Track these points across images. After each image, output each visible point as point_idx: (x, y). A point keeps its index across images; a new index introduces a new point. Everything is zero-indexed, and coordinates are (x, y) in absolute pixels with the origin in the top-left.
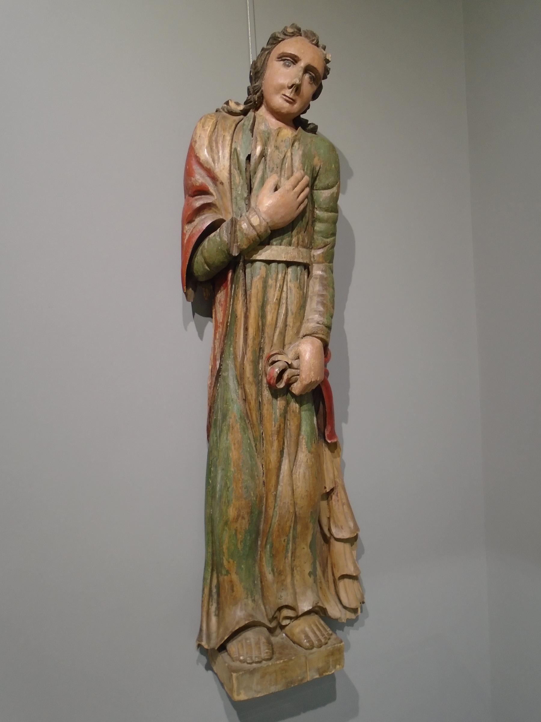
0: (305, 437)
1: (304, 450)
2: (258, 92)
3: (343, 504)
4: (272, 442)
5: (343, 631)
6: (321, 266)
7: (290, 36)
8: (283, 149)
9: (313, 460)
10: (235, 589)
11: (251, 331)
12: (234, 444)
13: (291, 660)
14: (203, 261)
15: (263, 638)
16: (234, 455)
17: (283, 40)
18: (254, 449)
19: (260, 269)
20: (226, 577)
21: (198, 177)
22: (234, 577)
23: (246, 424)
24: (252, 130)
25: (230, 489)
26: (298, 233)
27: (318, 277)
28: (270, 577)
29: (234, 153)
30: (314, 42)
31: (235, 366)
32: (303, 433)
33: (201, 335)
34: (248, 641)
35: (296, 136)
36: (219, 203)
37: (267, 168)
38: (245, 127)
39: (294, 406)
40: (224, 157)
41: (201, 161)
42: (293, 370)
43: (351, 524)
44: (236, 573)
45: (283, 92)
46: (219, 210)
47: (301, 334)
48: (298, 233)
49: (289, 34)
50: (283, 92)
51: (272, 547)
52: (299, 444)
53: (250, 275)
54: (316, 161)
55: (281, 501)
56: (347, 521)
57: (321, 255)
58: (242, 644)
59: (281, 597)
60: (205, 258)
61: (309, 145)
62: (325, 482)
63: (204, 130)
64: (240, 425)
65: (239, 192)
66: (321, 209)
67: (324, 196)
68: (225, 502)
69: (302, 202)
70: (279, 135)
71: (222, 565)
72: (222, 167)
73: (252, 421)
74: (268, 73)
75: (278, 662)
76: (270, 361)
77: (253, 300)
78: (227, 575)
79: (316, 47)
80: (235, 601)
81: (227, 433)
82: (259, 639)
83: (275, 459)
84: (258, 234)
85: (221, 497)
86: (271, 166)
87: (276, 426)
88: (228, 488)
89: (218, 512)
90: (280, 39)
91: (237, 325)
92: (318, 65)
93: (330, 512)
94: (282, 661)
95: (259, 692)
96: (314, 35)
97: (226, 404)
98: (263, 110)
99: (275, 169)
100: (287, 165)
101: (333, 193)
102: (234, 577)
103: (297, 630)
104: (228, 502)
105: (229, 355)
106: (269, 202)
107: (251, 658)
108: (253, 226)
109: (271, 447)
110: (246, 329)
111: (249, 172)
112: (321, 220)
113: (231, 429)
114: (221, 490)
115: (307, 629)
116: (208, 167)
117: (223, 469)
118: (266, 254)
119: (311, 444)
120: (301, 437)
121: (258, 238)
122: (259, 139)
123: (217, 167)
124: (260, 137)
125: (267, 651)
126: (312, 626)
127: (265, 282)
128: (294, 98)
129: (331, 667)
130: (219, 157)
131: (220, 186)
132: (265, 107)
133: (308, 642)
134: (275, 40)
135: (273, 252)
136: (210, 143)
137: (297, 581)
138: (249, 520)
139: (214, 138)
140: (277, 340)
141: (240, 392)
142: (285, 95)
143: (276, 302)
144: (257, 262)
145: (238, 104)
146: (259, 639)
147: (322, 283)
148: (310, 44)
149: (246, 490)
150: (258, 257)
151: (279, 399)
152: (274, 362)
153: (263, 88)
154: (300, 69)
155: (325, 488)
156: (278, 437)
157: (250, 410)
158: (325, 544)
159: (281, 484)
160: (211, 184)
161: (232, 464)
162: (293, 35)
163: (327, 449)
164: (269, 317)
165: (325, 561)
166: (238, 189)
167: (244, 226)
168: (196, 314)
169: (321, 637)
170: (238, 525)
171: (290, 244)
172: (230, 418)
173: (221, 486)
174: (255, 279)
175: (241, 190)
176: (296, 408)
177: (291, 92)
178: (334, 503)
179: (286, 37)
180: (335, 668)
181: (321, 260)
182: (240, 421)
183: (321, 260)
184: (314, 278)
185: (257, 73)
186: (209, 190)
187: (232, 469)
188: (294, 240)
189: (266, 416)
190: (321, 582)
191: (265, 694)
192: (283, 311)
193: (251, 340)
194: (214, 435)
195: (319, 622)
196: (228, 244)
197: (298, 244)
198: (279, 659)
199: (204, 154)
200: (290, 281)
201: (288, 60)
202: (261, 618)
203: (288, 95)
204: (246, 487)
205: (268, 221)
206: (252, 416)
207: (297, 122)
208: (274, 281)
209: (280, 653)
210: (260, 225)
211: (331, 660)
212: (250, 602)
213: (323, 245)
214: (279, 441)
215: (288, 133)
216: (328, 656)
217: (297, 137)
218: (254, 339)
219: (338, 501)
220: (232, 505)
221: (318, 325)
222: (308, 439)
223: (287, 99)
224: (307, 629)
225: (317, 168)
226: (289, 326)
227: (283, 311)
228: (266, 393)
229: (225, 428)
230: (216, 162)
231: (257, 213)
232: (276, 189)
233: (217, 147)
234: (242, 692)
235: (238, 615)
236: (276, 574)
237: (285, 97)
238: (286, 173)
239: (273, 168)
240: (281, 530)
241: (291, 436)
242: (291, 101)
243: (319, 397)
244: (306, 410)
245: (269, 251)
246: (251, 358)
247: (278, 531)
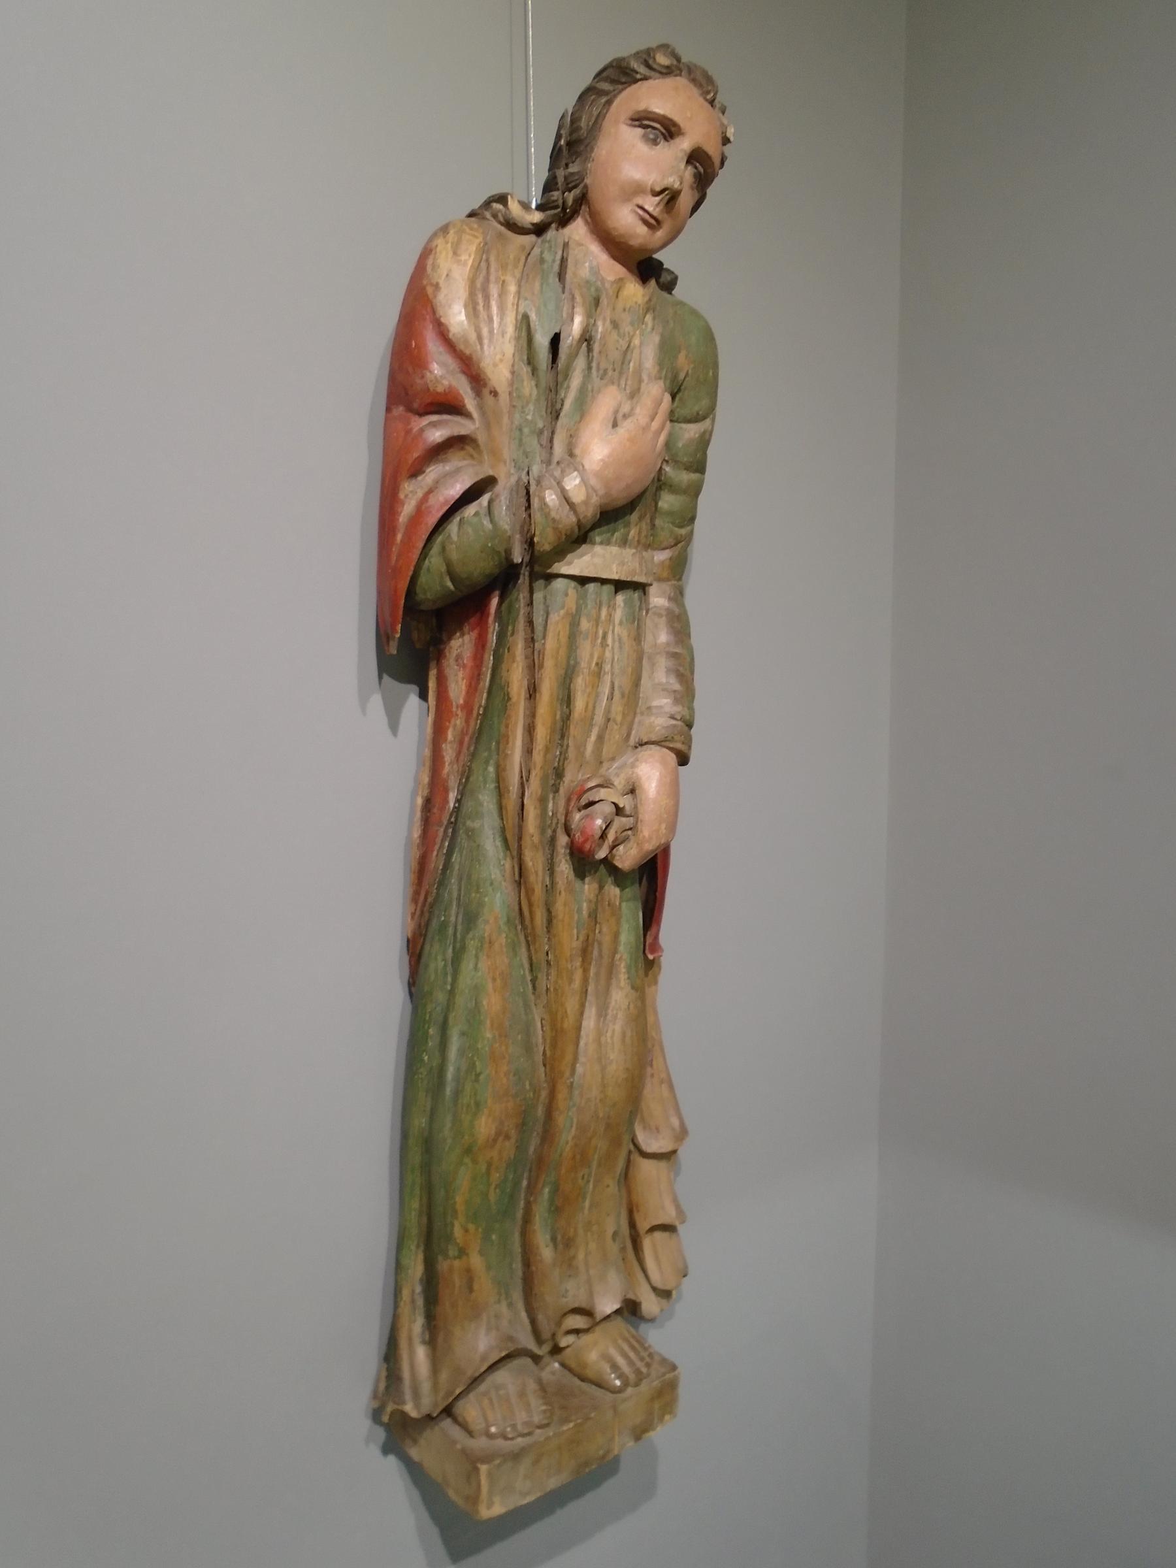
1: (622, 984)
2: (575, 187)
3: (662, 1082)
7: (661, 73)
8: (627, 328)
10: (476, 1287)
11: (541, 733)
12: (494, 980)
13: (589, 1419)
14: (444, 569)
15: (531, 1381)
16: (492, 1002)
17: (645, 78)
18: (530, 986)
19: (567, 595)
20: (457, 1263)
21: (436, 369)
22: (476, 1261)
23: (517, 935)
24: (561, 276)
25: (482, 1077)
26: (641, 518)
27: (664, 613)
29: (525, 325)
31: (501, 808)
32: (621, 948)
33: (394, 726)
34: (501, 1392)
36: (481, 438)
37: (594, 371)
38: (545, 266)
39: (613, 891)
40: (503, 334)
41: (451, 336)
43: (675, 1122)
44: (481, 1253)
46: (480, 452)
47: (633, 740)
48: (641, 518)
49: (655, 66)
50: (640, 201)
51: (555, 1190)
53: (542, 607)
54: (683, 361)
57: (667, 563)
58: (491, 1400)
59: (567, 1291)
60: (449, 565)
61: (671, 324)
63: (459, 262)
64: (507, 937)
65: (529, 417)
67: (687, 436)
68: (468, 1106)
71: (449, 1238)
72: (499, 356)
73: (533, 928)
74: (603, 148)
75: (565, 1428)
76: (583, 802)
77: (549, 663)
78: (459, 1257)
80: (476, 1312)
81: (477, 957)
84: (579, 521)
85: (457, 1093)
86: (603, 365)
87: (581, 938)
88: (478, 1075)
89: (448, 1125)
90: (638, 76)
91: (509, 716)
92: (712, 149)
94: (571, 1425)
95: (528, 1494)
96: (709, 80)
97: (477, 891)
98: (578, 229)
99: (610, 373)
100: (632, 364)
103: (593, 1356)
104: (477, 1104)
105: (485, 782)
106: (603, 447)
107: (514, 1426)
108: (567, 500)
109: (570, 984)
110: (530, 730)
113: (486, 945)
114: (457, 1079)
115: (613, 1352)
116: (467, 352)
117: (463, 1034)
118: (580, 563)
119: (637, 971)
120: (618, 956)
121: (576, 530)
122: (578, 299)
123: (486, 353)
124: (582, 296)
125: (544, 1408)
126: (620, 1341)
127: (574, 624)
128: (660, 218)
130: (491, 332)
131: (489, 400)
132: (586, 222)
133: (618, 1377)
134: (620, 74)
135: (597, 560)
136: (472, 295)
140: (593, 752)
141: (508, 864)
144: (560, 580)
145: (526, 206)
147: (672, 627)
148: (701, 100)
151: (587, 880)
152: (591, 804)
153: (588, 181)
154: (680, 155)
157: (530, 905)
159: (582, 1059)
160: (469, 390)
161: (488, 1022)
162: (668, 72)
164: (579, 704)
166: (526, 410)
167: (551, 497)
168: (386, 677)
169: (639, 1364)
170: (494, 1153)
171: (624, 543)
172: (487, 922)
173: (458, 1069)
174: (554, 618)
175: (534, 415)
179: (652, 73)
182: (506, 929)
184: (655, 613)
186: (464, 406)
187: (489, 1035)
189: (560, 917)
191: (539, 1494)
193: (542, 753)
194: (440, 958)
195: (628, 1331)
197: (639, 541)
199: (457, 317)
200: (621, 623)
201: (654, 128)
203: (650, 209)
206: (532, 919)
207: (647, 268)
209: (563, 1408)
210: (586, 503)
213: (672, 541)
215: (635, 291)
216: (652, 1399)
218: (547, 750)
220: (486, 1111)
221: (674, 722)
223: (647, 217)
224: (613, 1352)
225: (682, 376)
226: (615, 721)
228: (564, 867)
229: (472, 945)
230: (486, 341)
231: (581, 471)
232: (615, 425)
233: (487, 306)
234: (497, 1499)
236: (561, 1246)
237: (641, 212)
238: (629, 382)
239: (605, 371)
240: (578, 1157)
241: (601, 955)
242: (652, 221)
243: (652, 874)
244: (628, 901)
245: (587, 558)
247: (574, 1158)
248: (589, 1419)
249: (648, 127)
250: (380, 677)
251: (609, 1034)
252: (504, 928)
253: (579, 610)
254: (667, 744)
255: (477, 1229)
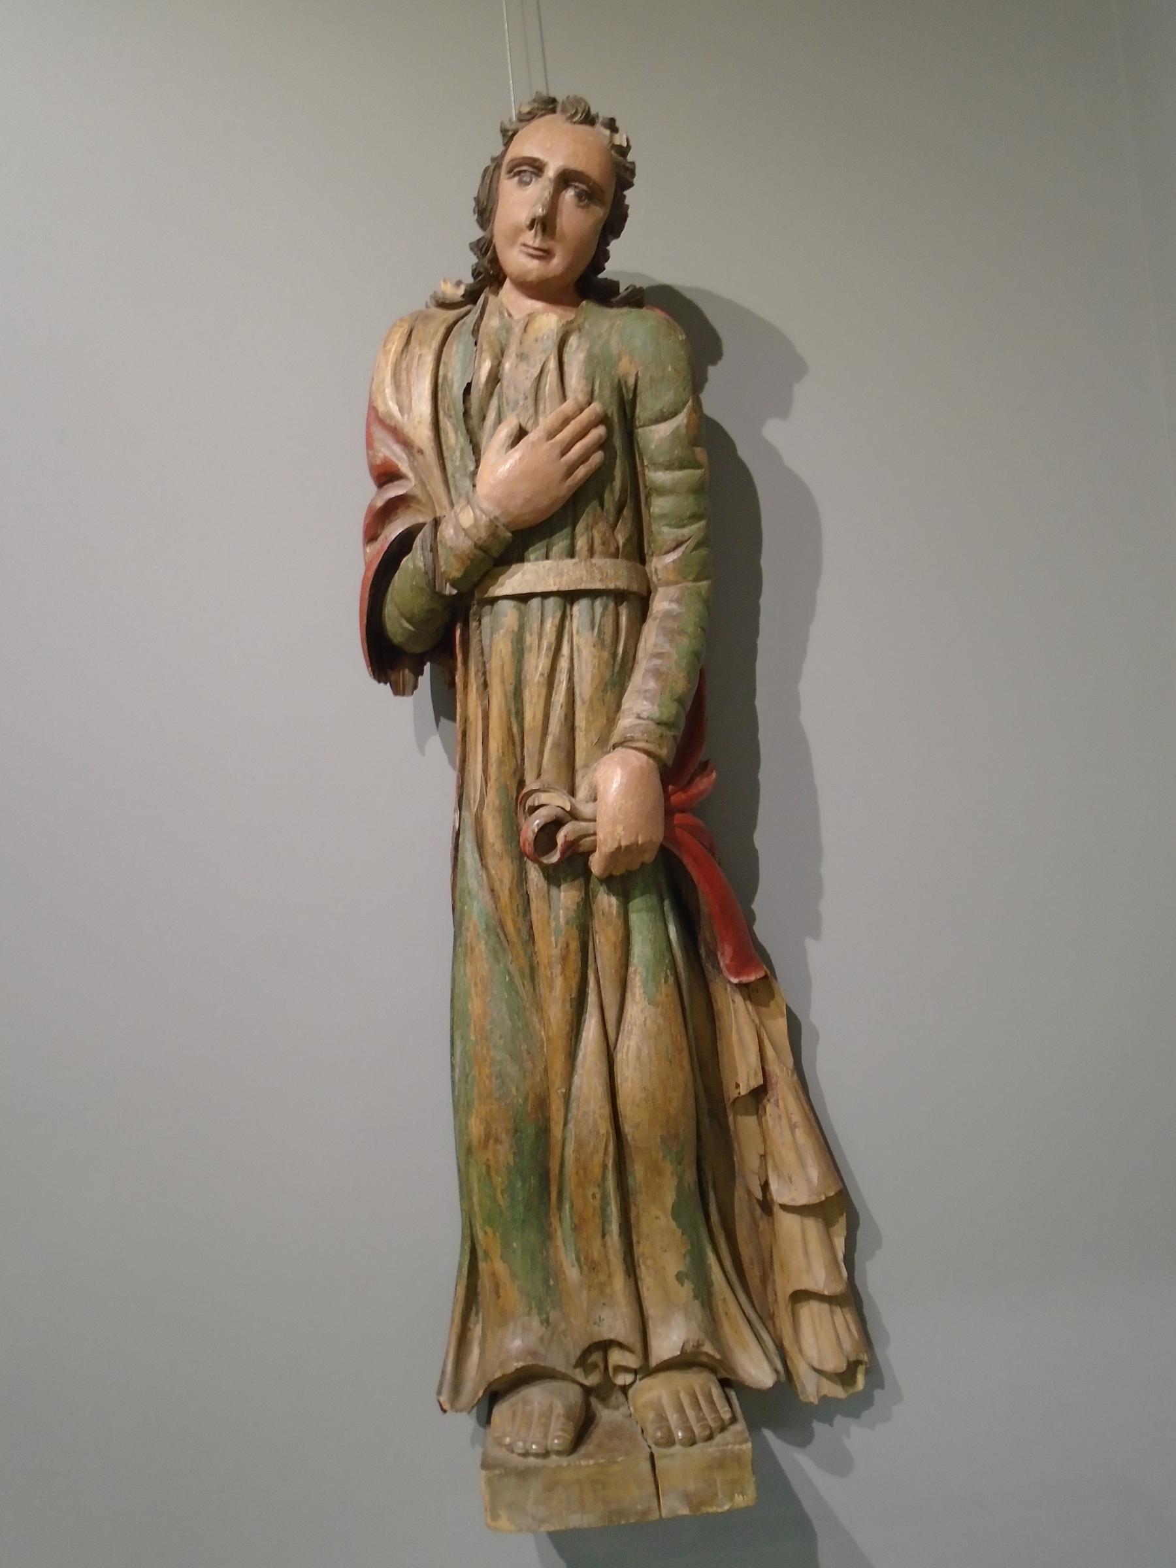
0: (640, 969)
1: (638, 997)
4: (552, 981)
5: (831, 1425)
6: (673, 591)
9: (660, 1020)
10: (502, 1292)
12: (476, 984)
28: (572, 1273)
30: (576, 119)
35: (571, 322)
39: (607, 902)
42: (584, 824)
45: (521, 240)
48: (589, 528)
52: (629, 984)
55: (578, 1108)
56: (803, 1166)
62: (736, 1074)
64: (486, 944)
66: (657, 466)
67: (657, 436)
69: (584, 458)
70: (529, 329)
75: (583, 1463)
79: (585, 128)
80: (504, 1318)
82: (551, 1407)
83: (559, 1015)
87: (559, 946)
92: (591, 164)
93: (765, 1141)
94: (591, 1462)
99: (521, 403)
101: (678, 428)
102: (500, 1266)
111: (466, 414)
112: (661, 491)
118: (517, 580)
120: (631, 969)
121: (477, 552)
125: (560, 1433)
128: (545, 246)
129: (720, 1495)
135: (527, 577)
137: (648, 1289)
138: (511, 1147)
139: (404, 365)
142: (525, 245)
143: (542, 679)
146: (551, 1407)
147: (664, 628)
148: (568, 125)
149: (499, 1081)
150: (498, 591)
151: (562, 887)
155: (738, 1086)
156: (563, 969)
158: (765, 1217)
159: (579, 1070)
163: (739, 999)
165: (767, 1255)
168: (443, 720)
171: (571, 554)
176: (610, 906)
177: (536, 235)
178: (770, 1123)
180: (732, 1499)
181: (672, 577)
183: (672, 577)
185: (485, 212)
187: (473, 1038)
188: (581, 543)
190: (724, 1300)
192: (560, 697)
196: (426, 573)
197: (591, 552)
198: (589, 1456)
202: (557, 1361)
203: (530, 243)
204: (499, 1075)
205: (497, 513)
208: (536, 636)
209: (599, 1445)
210: (476, 524)
211: (718, 1480)
212: (535, 1322)
214: (565, 979)
217: (575, 325)
219: (780, 1117)
222: (647, 971)
223: (531, 251)
225: (631, 381)
227: (560, 697)
234: (503, 1514)
235: (515, 1344)
236: (585, 1268)
237: (525, 249)
245: (518, 577)
246: (497, 802)
248: (616, 1462)
249: (520, 173)
250: (437, 721)
251: (625, 1050)
252: (483, 935)
253: (522, 627)
254: (630, 744)
255: (494, 1234)
